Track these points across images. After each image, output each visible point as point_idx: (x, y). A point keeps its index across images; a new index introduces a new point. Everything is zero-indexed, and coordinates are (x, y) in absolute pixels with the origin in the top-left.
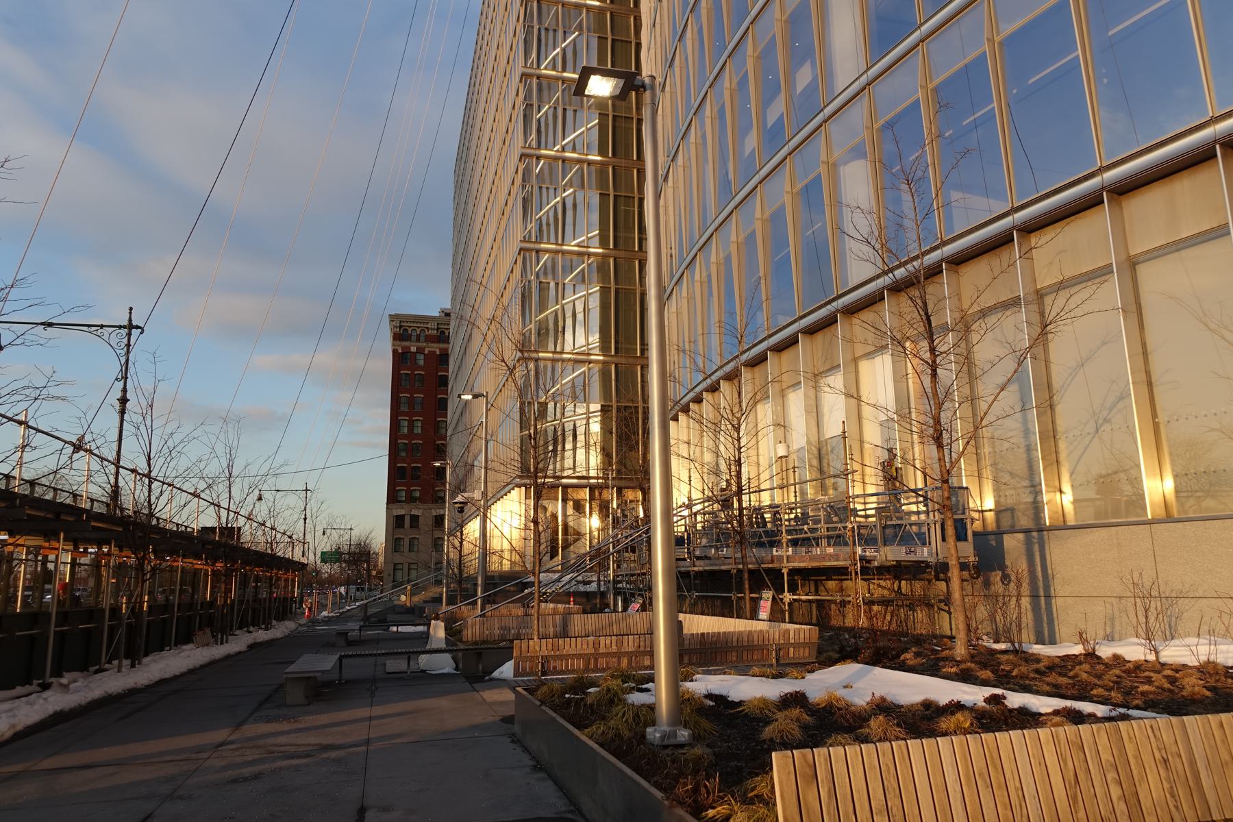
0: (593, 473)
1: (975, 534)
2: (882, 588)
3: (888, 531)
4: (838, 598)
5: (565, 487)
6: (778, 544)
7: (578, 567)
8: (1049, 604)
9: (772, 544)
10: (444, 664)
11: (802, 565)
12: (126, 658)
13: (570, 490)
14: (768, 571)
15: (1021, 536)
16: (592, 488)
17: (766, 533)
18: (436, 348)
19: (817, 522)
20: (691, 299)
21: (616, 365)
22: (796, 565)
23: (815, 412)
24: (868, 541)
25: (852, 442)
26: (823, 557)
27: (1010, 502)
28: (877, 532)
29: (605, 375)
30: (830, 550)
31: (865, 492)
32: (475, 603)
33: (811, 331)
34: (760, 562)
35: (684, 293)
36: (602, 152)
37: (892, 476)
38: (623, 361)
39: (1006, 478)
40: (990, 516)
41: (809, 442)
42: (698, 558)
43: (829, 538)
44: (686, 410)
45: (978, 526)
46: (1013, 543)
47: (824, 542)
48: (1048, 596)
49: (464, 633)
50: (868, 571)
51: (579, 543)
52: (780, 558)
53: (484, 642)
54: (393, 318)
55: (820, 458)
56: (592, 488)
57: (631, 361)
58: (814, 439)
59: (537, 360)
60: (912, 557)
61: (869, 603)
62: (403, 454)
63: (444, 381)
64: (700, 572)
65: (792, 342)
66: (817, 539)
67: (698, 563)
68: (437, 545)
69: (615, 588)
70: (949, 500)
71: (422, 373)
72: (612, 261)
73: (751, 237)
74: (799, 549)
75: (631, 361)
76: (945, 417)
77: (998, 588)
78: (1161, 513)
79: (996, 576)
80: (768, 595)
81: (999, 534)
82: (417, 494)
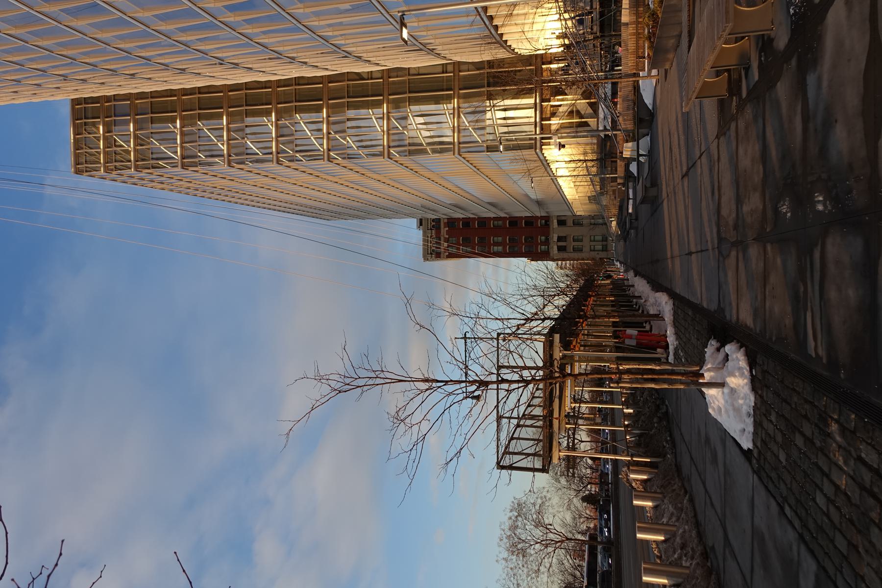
0: (532, 101)
5: (542, 119)
7: (594, 106)
10: (645, 142)
12: (637, 343)
16: (542, 100)
18: (444, 230)
20: (427, 29)
29: (466, 97)
32: (615, 135)
35: (424, 33)
36: (318, 110)
38: (457, 83)
42: (592, 7)
53: (634, 117)
54: (426, 259)
56: (542, 100)
57: (457, 78)
62: (516, 249)
63: (467, 222)
67: (594, 7)
68: (578, 221)
69: (609, 71)
71: (462, 234)
72: (391, 97)
75: (457, 78)
82: (543, 238)
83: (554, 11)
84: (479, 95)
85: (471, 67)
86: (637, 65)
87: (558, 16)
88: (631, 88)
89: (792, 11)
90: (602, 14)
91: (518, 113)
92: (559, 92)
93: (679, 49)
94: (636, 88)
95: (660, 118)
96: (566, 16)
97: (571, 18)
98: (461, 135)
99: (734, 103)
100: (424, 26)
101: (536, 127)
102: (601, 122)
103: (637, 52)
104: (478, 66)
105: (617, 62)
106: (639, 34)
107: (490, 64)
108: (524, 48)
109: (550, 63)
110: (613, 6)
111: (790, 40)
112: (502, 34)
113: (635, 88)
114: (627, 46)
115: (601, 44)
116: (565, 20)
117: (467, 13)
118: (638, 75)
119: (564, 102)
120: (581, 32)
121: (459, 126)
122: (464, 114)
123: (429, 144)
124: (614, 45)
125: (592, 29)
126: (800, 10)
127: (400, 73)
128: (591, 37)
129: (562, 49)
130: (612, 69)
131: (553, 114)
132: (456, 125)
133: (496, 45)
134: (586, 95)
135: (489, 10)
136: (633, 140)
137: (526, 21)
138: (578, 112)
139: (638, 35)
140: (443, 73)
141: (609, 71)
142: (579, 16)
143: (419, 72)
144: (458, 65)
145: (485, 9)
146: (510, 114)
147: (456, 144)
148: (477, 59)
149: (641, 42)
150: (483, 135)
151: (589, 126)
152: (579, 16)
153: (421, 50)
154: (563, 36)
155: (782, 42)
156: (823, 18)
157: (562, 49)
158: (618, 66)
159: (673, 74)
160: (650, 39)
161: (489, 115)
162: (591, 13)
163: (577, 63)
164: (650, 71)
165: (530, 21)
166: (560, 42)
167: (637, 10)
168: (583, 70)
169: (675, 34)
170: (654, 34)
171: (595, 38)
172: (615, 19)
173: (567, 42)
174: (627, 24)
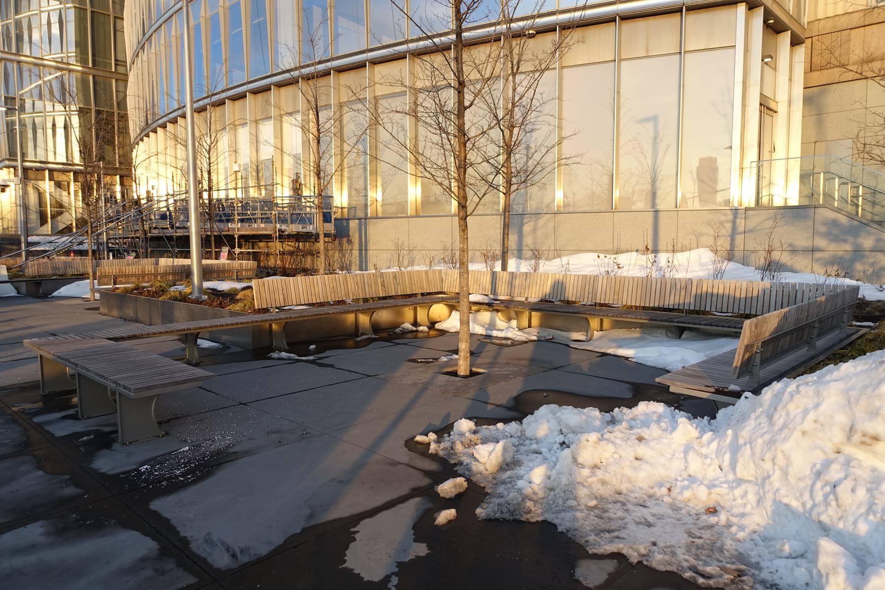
1: (336, 219)
2: (289, 246)
3: (294, 216)
4: (266, 251)
5: (51, 171)
6: (233, 221)
7: (68, 230)
8: (366, 254)
9: (228, 221)
11: (247, 233)
13: (55, 173)
14: (226, 236)
15: (357, 221)
16: (76, 173)
17: (225, 214)
19: (255, 208)
20: (168, 46)
21: (94, 76)
22: (243, 233)
23: (256, 141)
24: (283, 221)
25: (277, 165)
26: (258, 229)
27: (354, 203)
28: (288, 217)
29: (84, 83)
30: (263, 225)
31: (283, 193)
32: (20, 255)
33: (255, 92)
34: (220, 231)
35: (162, 42)
37: (297, 188)
38: (101, 73)
39: (354, 193)
40: (346, 210)
41: (251, 161)
43: (262, 219)
44: (164, 126)
45: (338, 215)
46: (353, 224)
47: (259, 221)
48: (366, 250)
49: (26, 271)
50: (283, 237)
51: (66, 214)
52: (233, 229)
53: (44, 276)
55: (258, 172)
56: (76, 173)
57: (108, 75)
58: (254, 160)
59: (19, 62)
60: (305, 230)
61: (283, 254)
64: (181, 237)
65: (243, 96)
66: (255, 220)
67: (178, 231)
69: (108, 247)
70: (324, 199)
73: (215, 18)
74: (244, 224)
75: (108, 75)
76: (322, 163)
77: (345, 245)
78: (414, 213)
79: (345, 240)
80: (225, 250)
81: (348, 220)
83: (177, 189)
84: (87, 100)
85: (121, 95)
86: (106, 276)
87: (171, 192)
88: (81, 271)
89: (143, 469)
90: (170, 238)
91: (59, 139)
92: (87, 190)
93: (122, 321)
94: (81, 277)
95: (37, 306)
96: (171, 201)
97: (167, 207)
98: (32, 67)
99: (28, 406)
100: (170, 43)
101: (41, 162)
102: (43, 237)
103: (122, 276)
104: (122, 104)
105: (118, 254)
106: (143, 277)
107: (124, 118)
108: (139, 154)
109: (122, 184)
110: (177, 250)
111: (104, 475)
112: (156, 132)
113: (82, 275)
114: (133, 264)
115: (138, 238)
116: (167, 200)
117: (181, 92)
118: (95, 278)
119: (73, 199)
120: (153, 217)
121: (44, 66)
122: (62, 76)
123: (18, 24)
124: (136, 252)
125: (155, 228)
126: (145, 481)
127: (118, 7)
128: (146, 227)
129: (136, 197)
130: (110, 250)
131: (58, 185)
132: (46, 62)
133: (143, 124)
134: (81, 223)
135: (183, 120)
136: (10, 277)
137: (168, 157)
138: (61, 213)
139: (143, 275)
140: (116, 60)
141: (108, 247)
142: (170, 213)
143: (118, 31)
144: (123, 79)
145: (184, 116)
146: (60, 132)
147: (18, 58)
148: (130, 103)
149: (134, 279)
150: (32, 96)
151: (42, 224)
152: (170, 213)
153: (144, 34)
154: (149, 199)
155: (107, 463)
156: (126, 525)
157: (136, 197)
158: (114, 256)
159: (95, 317)
160: (136, 289)
161: (59, 107)
162: (172, 227)
163: (118, 212)
164: (99, 291)
165: (168, 161)
166: (143, 195)
167: (169, 274)
168: (110, 219)
169: (139, 315)
170: (141, 293)
171: (145, 232)
172: (164, 252)
173: (143, 202)
174: (157, 263)
